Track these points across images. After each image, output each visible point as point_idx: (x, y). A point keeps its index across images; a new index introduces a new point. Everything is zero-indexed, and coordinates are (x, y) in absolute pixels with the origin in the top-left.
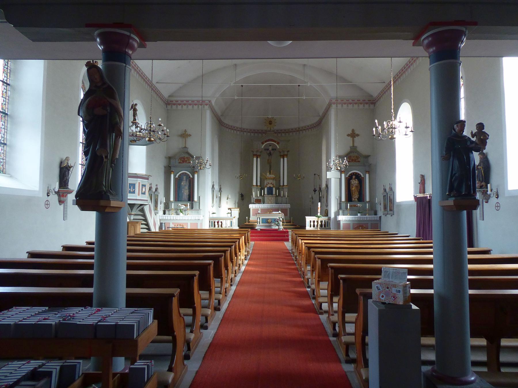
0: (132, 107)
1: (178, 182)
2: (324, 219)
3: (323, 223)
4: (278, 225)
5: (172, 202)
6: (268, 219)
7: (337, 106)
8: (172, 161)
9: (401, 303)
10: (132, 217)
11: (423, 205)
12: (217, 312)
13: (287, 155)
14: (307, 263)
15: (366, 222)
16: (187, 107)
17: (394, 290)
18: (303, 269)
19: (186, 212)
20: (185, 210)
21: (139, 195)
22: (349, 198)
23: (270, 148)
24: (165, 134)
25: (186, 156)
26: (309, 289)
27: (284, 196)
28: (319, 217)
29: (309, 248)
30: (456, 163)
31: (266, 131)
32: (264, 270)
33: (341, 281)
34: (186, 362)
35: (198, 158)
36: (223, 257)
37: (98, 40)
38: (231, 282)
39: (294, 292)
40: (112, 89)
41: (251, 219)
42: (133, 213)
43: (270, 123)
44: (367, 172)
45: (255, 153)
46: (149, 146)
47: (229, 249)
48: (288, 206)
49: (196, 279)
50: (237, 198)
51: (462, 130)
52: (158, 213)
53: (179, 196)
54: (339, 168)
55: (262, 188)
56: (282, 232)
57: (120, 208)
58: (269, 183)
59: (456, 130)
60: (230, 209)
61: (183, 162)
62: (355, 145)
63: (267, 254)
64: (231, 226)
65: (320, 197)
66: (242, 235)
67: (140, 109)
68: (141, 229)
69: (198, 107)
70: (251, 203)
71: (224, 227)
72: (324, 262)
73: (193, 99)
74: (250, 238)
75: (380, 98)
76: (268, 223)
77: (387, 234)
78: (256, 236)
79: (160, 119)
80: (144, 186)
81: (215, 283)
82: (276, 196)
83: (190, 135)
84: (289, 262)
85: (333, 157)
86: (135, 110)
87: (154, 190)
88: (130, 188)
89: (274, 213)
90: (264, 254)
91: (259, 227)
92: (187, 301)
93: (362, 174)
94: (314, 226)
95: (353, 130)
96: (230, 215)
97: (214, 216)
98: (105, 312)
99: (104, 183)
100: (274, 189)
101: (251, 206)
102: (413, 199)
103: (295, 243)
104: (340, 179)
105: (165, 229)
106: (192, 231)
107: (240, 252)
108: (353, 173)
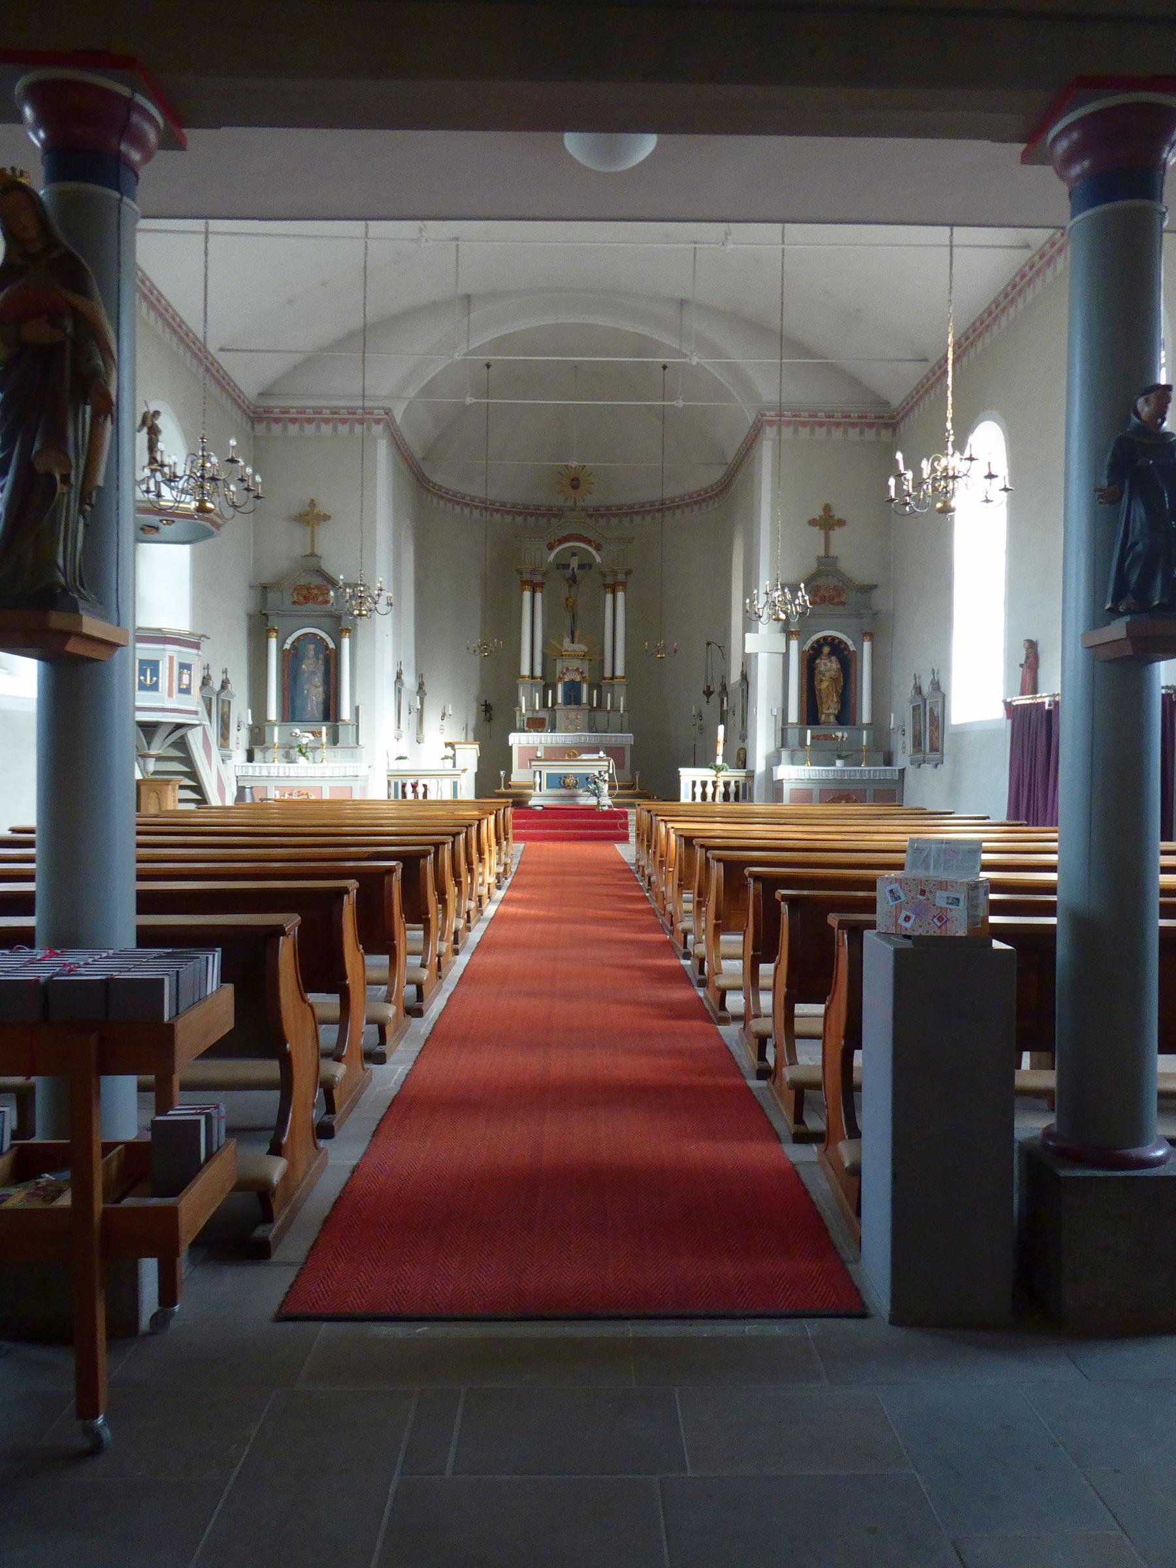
0: (144, 422)
1: (291, 662)
2: (733, 775)
3: (732, 788)
4: (596, 794)
5: (272, 724)
6: (566, 776)
7: (779, 432)
8: (272, 597)
9: (962, 932)
10: (152, 765)
11: (1032, 730)
12: (415, 1021)
13: (624, 584)
14: (683, 885)
15: (860, 787)
17: (940, 898)
18: (670, 907)
19: (318, 752)
20: (314, 749)
21: (170, 695)
22: (811, 714)
24: (248, 490)
25: (316, 581)
26: (689, 962)
27: (615, 708)
30: (1139, 511)
31: (561, 509)
32: (554, 913)
33: (784, 907)
34: (322, 1143)
37: (28, 112)
38: (456, 942)
40: (80, 262)
42: (152, 752)
44: (865, 634)
45: (526, 577)
46: (198, 545)
48: (627, 739)
50: (472, 716)
51: (1161, 414)
52: (230, 757)
53: (294, 709)
54: (783, 616)
55: (548, 685)
56: (609, 814)
57: (113, 646)
58: (571, 669)
59: (1143, 415)
60: (450, 745)
62: (833, 552)
63: (563, 873)
67: (167, 424)
68: (176, 801)
69: (352, 430)
70: (515, 730)
73: (335, 403)
75: (912, 408)
76: (565, 786)
77: (922, 813)
78: (531, 827)
79: (233, 442)
80: (184, 666)
81: (409, 936)
82: (592, 709)
83: (326, 518)
84: (630, 906)
85: (765, 583)
86: (154, 432)
87: (217, 686)
88: (143, 673)
89: (584, 757)
91: (536, 801)
92: (323, 970)
93: (850, 643)
95: (827, 508)
97: (403, 765)
98: (73, 958)
99: (60, 562)
100: (585, 687)
101: (515, 739)
102: (1000, 713)
103: (647, 837)
104: (786, 656)
105: (253, 798)
106: (335, 805)
107: (481, 860)
108: (825, 638)
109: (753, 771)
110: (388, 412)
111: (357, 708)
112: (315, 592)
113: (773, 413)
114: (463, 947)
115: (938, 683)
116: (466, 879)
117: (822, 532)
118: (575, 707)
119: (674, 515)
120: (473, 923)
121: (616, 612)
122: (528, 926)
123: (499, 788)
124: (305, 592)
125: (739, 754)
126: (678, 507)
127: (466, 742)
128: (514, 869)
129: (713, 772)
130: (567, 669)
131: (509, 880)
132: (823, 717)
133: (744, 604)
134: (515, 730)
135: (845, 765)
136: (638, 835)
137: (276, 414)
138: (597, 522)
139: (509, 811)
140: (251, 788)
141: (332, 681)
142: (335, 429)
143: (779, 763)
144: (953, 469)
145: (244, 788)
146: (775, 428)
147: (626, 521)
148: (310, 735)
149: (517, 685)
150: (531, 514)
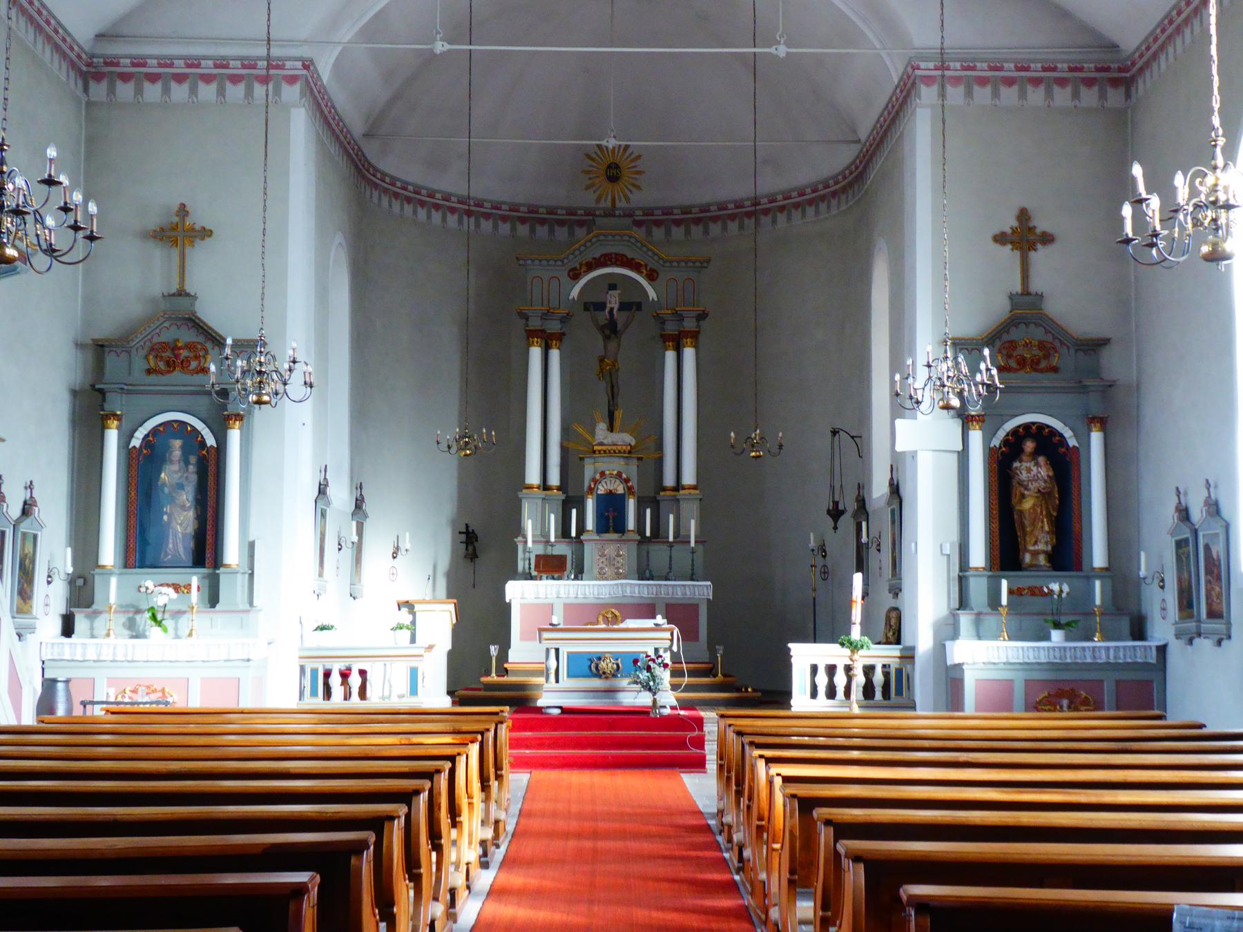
1: (142, 467)
2: (881, 655)
3: (878, 678)
7: (943, 95)
8: (110, 360)
13: (695, 336)
14: (798, 881)
18: (774, 914)
19: (184, 621)
20: (178, 613)
22: (1007, 552)
24: (75, 228)
25: (187, 336)
27: (681, 539)
45: (535, 323)
52: (32, 629)
53: (144, 542)
56: (672, 722)
58: (607, 474)
62: (1036, 285)
63: (595, 835)
69: (249, 92)
75: (1155, 56)
76: (599, 674)
78: (540, 744)
79: (52, 152)
82: (643, 540)
83: (206, 233)
85: (926, 345)
91: (551, 698)
93: (1067, 433)
95: (1023, 215)
97: (325, 638)
100: (631, 504)
103: (736, 778)
107: (455, 824)
108: (1027, 427)
109: (913, 649)
110: (307, 65)
111: (252, 546)
113: (931, 65)
115: (1216, 504)
116: (428, 857)
117: (1017, 253)
119: (774, 222)
121: (682, 379)
123: (488, 673)
124: (168, 354)
125: (888, 618)
127: (435, 601)
128: (510, 828)
129: (847, 652)
130: (603, 474)
131: (503, 849)
132: (1027, 558)
134: (514, 575)
135: (1068, 639)
136: (721, 767)
137: (125, 66)
140: (67, 682)
142: (221, 92)
143: (955, 635)
144: (1226, 192)
145: (54, 681)
146: (935, 89)
147: (697, 231)
148: (171, 591)
149: (520, 501)
150: (542, 222)
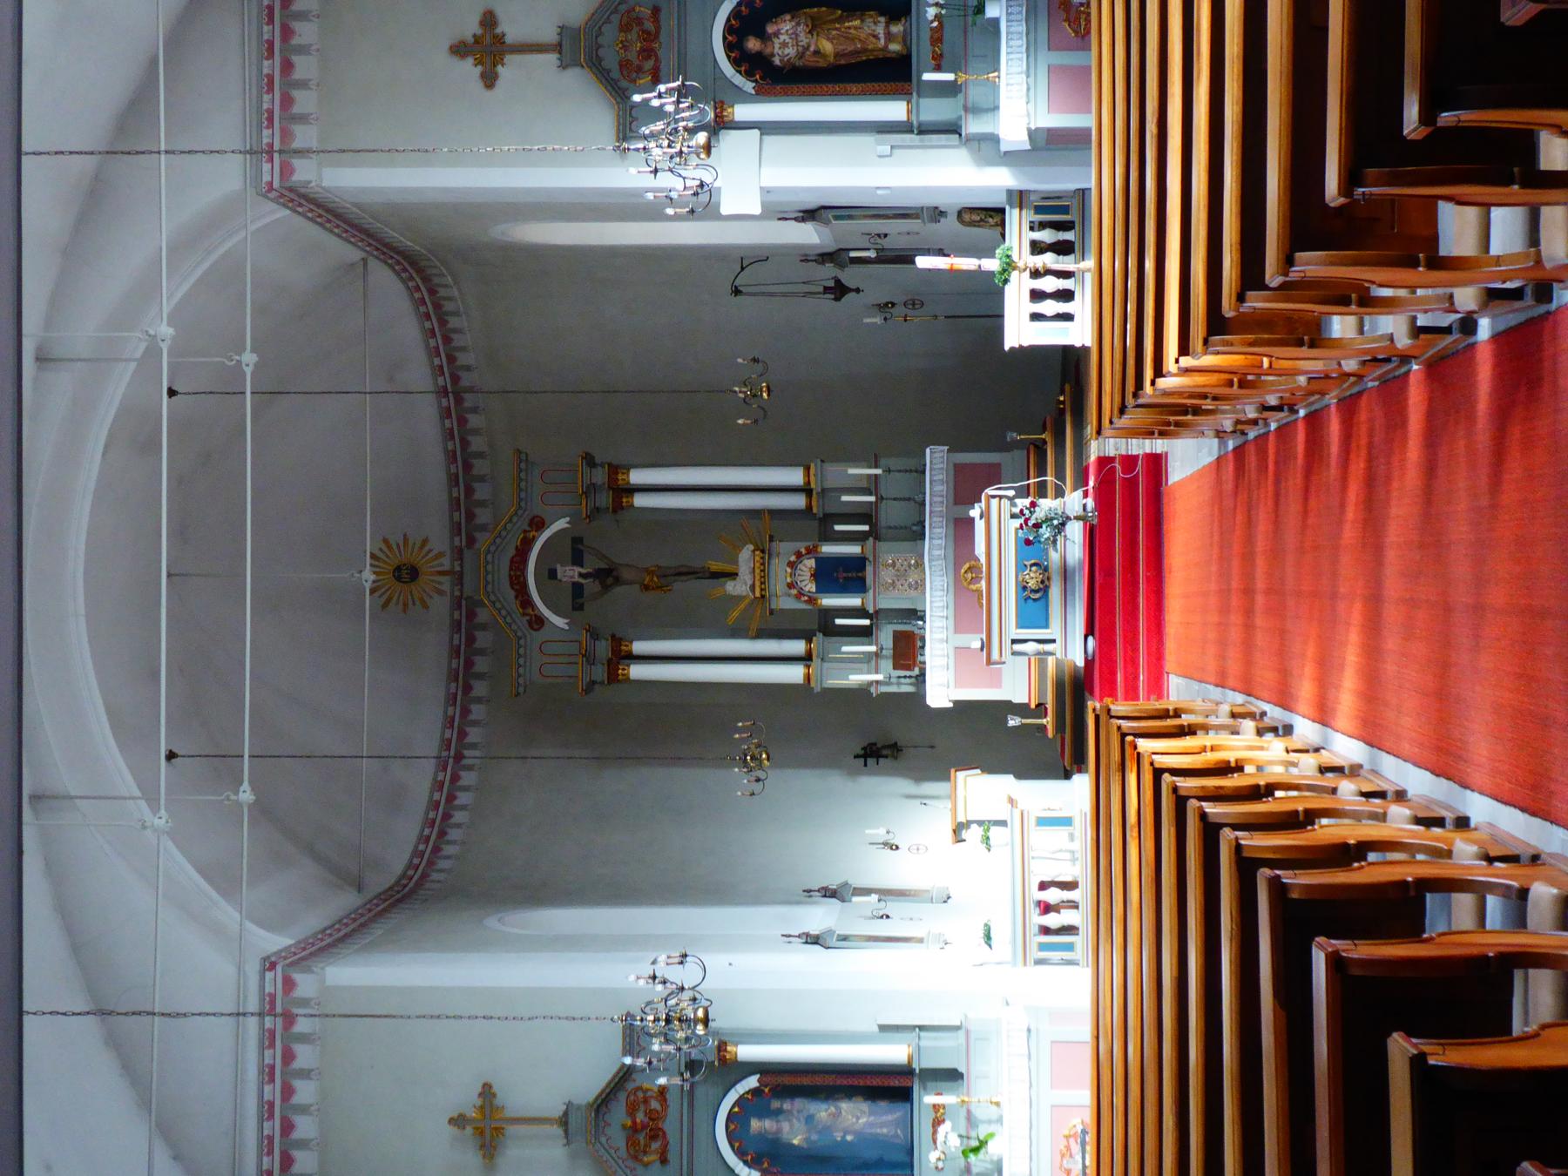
2: (1019, 231)
3: (1047, 236)
13: (615, 470)
14: (1311, 335)
16: (304, 1110)
18: (1350, 365)
19: (978, 1112)
20: (970, 1120)
22: (889, 74)
23: (569, 573)
25: (618, 1114)
27: (872, 485)
28: (1009, 266)
29: (1217, 324)
31: (457, 604)
33: (1446, 118)
35: (633, 1038)
36: (1287, 877)
38: (1439, 822)
39: (1503, 413)
41: (1020, 697)
43: (406, 573)
45: (600, 672)
47: (1227, 835)
48: (936, 459)
49: (1443, 1056)
54: (702, 137)
58: (791, 580)
60: (958, 830)
61: (656, 1134)
62: (549, 35)
63: (1248, 592)
64: (1067, 821)
65: (879, 260)
66: (1127, 755)
69: (305, 1038)
70: (919, 696)
71: (1079, 868)
72: (1311, 224)
74: (1145, 704)
76: (1044, 589)
78: (1132, 662)
81: (1457, 925)
82: (875, 534)
83: (487, 1092)
84: (1334, 448)
90: (1248, 612)
91: (1074, 649)
94: (1066, 296)
95: (459, 50)
96: (995, 832)
100: (828, 549)
101: (939, 695)
103: (1176, 416)
104: (767, 128)
107: (1239, 768)
108: (729, 47)
109: (1010, 192)
110: (269, 964)
111: (884, 1028)
112: (640, 1117)
113: (266, 167)
114: (1448, 808)
117: (508, 58)
118: (869, 569)
119: (468, 368)
120: (1384, 786)
121: (670, 486)
122: (1390, 668)
124: (641, 1137)
125: (972, 224)
126: (451, 359)
127: (953, 797)
128: (1240, 698)
130: (791, 586)
131: (1267, 707)
132: (895, 47)
133: (676, 218)
136: (1163, 434)
138: (483, 528)
139: (1119, 708)
141: (829, 1080)
142: (305, 1074)
143: (994, 139)
146: (297, 162)
147: (480, 467)
148: (942, 1130)
